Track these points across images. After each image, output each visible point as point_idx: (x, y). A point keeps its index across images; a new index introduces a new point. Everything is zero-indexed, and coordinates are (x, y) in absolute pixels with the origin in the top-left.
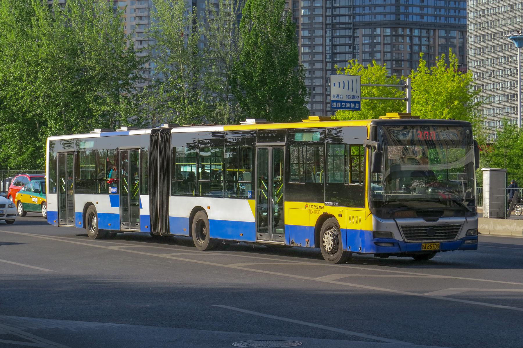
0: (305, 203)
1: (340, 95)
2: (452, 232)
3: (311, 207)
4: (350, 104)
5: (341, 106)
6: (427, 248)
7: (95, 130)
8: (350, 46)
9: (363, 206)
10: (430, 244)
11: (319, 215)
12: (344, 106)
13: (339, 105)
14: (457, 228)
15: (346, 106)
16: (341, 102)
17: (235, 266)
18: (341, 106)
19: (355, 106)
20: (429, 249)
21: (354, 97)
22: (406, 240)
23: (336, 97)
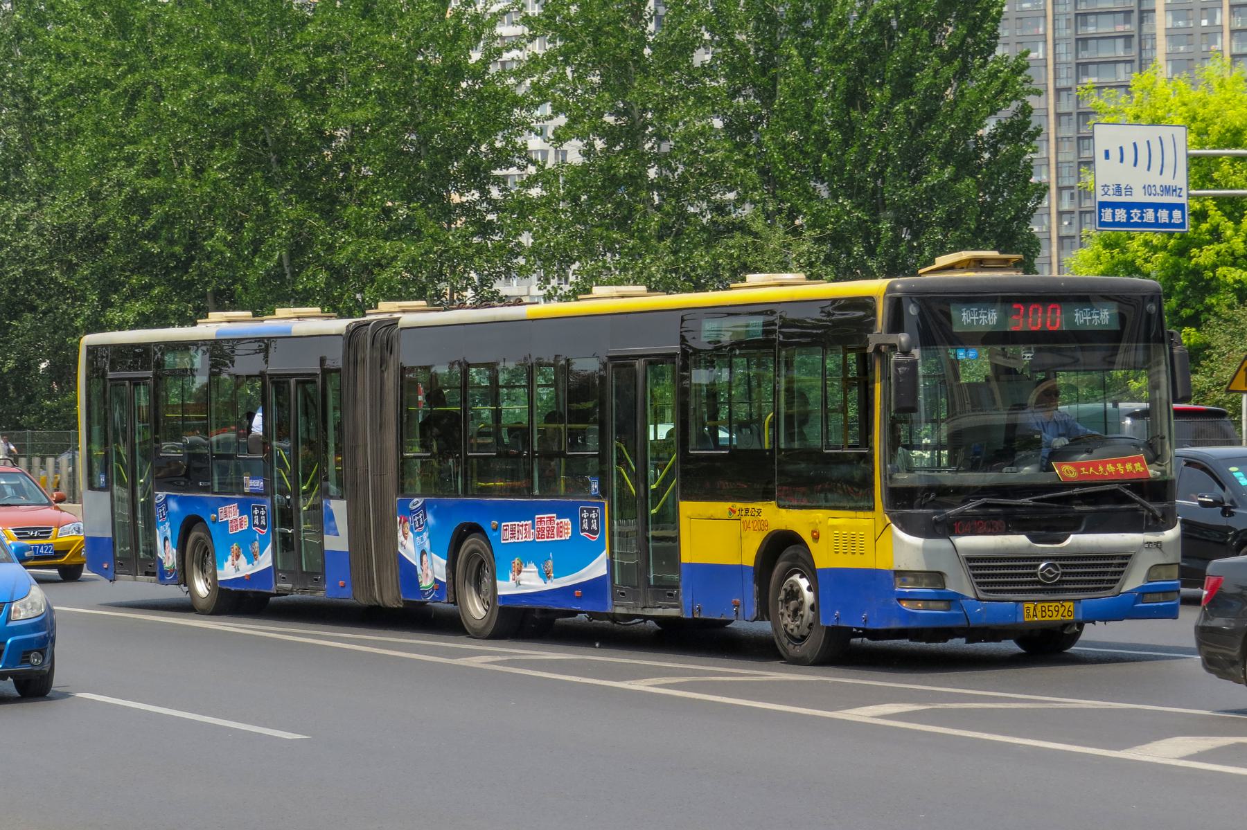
0: (730, 504)
1: (1123, 186)
2: (1105, 573)
3: (743, 513)
4: (1156, 212)
5: (1129, 218)
6: (1039, 615)
7: (210, 314)
8: (1128, 38)
9: (872, 509)
10: (1046, 605)
11: (766, 533)
12: (1136, 219)
13: (1121, 215)
14: (1122, 560)
15: (1142, 218)
16: (1128, 206)
17: (475, 662)
18: (1129, 218)
19: (1170, 217)
20: (1047, 618)
21: (1167, 190)
22: (981, 596)
23: (1111, 192)
